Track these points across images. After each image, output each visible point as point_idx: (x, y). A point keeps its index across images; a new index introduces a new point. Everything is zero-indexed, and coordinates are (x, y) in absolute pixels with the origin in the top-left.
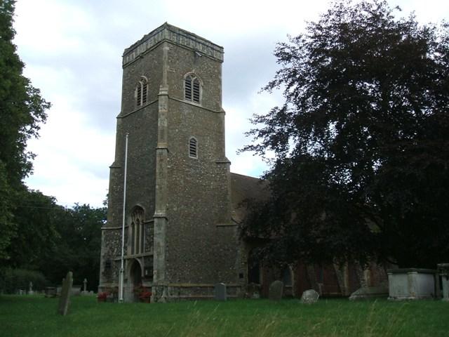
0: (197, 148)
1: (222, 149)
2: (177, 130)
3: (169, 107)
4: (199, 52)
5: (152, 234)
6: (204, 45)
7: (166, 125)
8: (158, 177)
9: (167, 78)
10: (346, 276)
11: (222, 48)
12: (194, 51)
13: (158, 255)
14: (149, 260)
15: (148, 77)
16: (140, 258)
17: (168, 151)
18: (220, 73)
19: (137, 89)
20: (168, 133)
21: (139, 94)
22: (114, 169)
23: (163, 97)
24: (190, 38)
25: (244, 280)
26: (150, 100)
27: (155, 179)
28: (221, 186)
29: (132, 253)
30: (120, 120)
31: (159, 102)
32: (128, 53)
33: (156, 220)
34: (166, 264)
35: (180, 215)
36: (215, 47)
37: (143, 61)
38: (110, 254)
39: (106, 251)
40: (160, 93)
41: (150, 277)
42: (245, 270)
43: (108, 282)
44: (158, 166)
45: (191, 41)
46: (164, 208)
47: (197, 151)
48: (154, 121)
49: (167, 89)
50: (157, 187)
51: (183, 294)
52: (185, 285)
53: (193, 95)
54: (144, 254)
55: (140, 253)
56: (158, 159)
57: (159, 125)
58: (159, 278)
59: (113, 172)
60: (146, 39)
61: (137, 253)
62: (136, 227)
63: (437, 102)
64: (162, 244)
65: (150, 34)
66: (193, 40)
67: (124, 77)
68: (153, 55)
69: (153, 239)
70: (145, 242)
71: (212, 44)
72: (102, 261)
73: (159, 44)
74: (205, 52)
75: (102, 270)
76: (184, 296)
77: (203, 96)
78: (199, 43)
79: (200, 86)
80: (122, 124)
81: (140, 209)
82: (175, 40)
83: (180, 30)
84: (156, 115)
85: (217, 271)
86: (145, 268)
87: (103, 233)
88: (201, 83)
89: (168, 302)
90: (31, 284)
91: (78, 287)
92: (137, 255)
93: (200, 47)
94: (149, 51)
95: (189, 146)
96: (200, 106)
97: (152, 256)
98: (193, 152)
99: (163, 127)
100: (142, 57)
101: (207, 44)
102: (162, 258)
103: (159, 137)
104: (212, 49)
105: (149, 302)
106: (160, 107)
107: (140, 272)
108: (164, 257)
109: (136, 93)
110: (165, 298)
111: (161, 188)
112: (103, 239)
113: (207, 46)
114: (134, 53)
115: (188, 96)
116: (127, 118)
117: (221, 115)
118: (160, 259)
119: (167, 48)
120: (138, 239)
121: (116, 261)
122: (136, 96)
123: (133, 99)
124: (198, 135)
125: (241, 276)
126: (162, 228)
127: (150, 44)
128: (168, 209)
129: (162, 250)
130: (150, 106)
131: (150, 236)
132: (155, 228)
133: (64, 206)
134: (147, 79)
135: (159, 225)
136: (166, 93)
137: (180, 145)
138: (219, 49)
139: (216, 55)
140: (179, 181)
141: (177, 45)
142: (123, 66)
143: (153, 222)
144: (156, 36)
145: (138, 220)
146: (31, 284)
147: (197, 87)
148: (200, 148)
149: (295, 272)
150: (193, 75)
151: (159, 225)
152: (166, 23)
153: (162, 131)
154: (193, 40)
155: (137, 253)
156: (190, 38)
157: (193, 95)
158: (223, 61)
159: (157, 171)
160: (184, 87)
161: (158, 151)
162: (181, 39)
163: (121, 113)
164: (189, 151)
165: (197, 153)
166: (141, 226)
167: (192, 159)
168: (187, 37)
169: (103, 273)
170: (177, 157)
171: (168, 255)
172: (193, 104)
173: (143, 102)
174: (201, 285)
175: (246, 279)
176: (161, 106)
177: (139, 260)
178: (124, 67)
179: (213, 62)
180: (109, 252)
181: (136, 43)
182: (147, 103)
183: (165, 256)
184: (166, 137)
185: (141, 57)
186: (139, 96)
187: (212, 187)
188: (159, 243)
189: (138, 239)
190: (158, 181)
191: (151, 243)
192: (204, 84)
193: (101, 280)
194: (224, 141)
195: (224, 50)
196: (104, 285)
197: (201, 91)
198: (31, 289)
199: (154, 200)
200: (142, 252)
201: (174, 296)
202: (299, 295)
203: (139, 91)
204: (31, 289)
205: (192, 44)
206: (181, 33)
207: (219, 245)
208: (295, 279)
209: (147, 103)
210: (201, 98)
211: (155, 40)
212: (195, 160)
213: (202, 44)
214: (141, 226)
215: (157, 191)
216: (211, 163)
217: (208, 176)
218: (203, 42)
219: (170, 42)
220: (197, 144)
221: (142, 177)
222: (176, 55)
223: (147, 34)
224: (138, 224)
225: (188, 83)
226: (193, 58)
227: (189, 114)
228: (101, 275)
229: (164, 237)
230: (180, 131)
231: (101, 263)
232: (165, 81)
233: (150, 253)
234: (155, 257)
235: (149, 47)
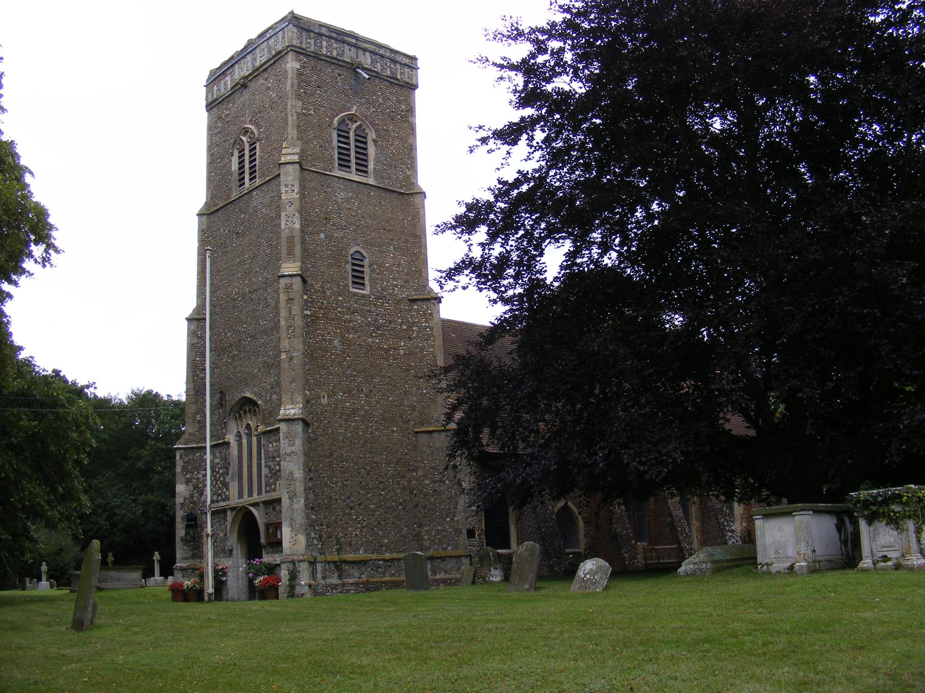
0: (366, 270)
1: (420, 271)
2: (322, 236)
3: (303, 187)
4: (363, 69)
5: (275, 457)
6: (377, 54)
7: (297, 226)
8: (283, 335)
9: (304, 126)
10: (696, 524)
11: (414, 59)
12: (353, 68)
13: (290, 498)
14: (274, 509)
15: (258, 126)
16: (255, 505)
17: (304, 281)
18: (411, 110)
19: (236, 154)
20: (303, 242)
21: (241, 163)
22: (195, 323)
23: (289, 168)
24: (344, 42)
25: (476, 541)
26: (263, 175)
27: (279, 339)
28: (422, 349)
29: (241, 496)
30: (205, 218)
31: (282, 178)
32: (216, 77)
33: (283, 427)
34: (308, 516)
35: (334, 414)
36: (399, 58)
37: (246, 94)
38: (195, 499)
39: (187, 495)
40: (283, 160)
41: (277, 545)
42: (480, 521)
43: (194, 556)
44: (283, 313)
45: (347, 48)
46: (299, 399)
47: (367, 278)
48: (273, 219)
49: (298, 150)
50: (283, 356)
51: (349, 576)
52: (350, 557)
53: (353, 160)
54: (265, 497)
55: (255, 495)
56: (283, 298)
57: (283, 226)
58: (293, 540)
59: (192, 327)
60: (250, 48)
61: (250, 495)
62: (245, 441)
63: (559, 188)
64: (299, 474)
65: (261, 35)
66: (349, 44)
67: (210, 128)
68: (266, 79)
69: (279, 465)
70: (265, 471)
71: (392, 51)
72: (180, 514)
73: (279, 56)
74: (378, 68)
75: (180, 532)
76: (351, 581)
77: (377, 161)
78: (365, 50)
79: (369, 139)
80: (209, 227)
81: (252, 403)
82: (313, 48)
83: (321, 25)
84: (276, 205)
85: (420, 526)
86: (268, 526)
87: (178, 457)
88: (372, 135)
89: (315, 593)
90: (44, 568)
91: (137, 569)
92: (256, 497)
93: (366, 60)
94: (258, 72)
95: (349, 267)
96: (371, 181)
97: (279, 501)
98: (359, 280)
99: (292, 229)
100: (244, 86)
101: (382, 52)
102: (300, 504)
103: (284, 251)
104: (395, 62)
105: (277, 597)
106: (283, 189)
107: (255, 535)
108: (303, 500)
109: (235, 161)
110: (310, 586)
111: (291, 359)
112: (178, 469)
113: (382, 56)
114: (228, 78)
115: (344, 164)
116: (219, 214)
117: (417, 199)
118: (296, 506)
119: (297, 65)
120: (250, 467)
121: (267, 503)
122: (235, 166)
123: (230, 173)
124: (368, 244)
125: (471, 534)
126: (298, 442)
127: (261, 57)
128: (308, 402)
129: (299, 487)
130: (264, 188)
131: (274, 458)
132: (284, 443)
133: (113, 395)
134: (256, 132)
135: (290, 436)
136: (296, 158)
137: (330, 266)
138: (407, 61)
139: (402, 74)
140: (331, 341)
141: (316, 56)
142: (207, 106)
143: (278, 429)
144: (271, 42)
145: (248, 425)
146: (44, 568)
147: (361, 141)
148: (373, 271)
149: (586, 522)
150: (352, 118)
151: (290, 436)
152: (292, 13)
153: (290, 239)
154: (349, 44)
155: (250, 495)
156: (266, 69)
157: (353, 160)
158: (416, 87)
159: (283, 323)
160: (335, 143)
161: (283, 282)
162: (324, 43)
163: (206, 203)
164: (350, 279)
165: (367, 282)
166: (254, 439)
167: (355, 294)
168: (336, 40)
169: (182, 540)
170: (324, 292)
171: (311, 496)
172: (357, 178)
173: (251, 180)
174: (388, 556)
175: (480, 536)
176: (286, 186)
177: (251, 508)
178: (210, 106)
179: (395, 89)
180: (192, 496)
181: (232, 58)
182: (258, 182)
183: (307, 499)
184: (298, 249)
185: (243, 85)
186: (241, 167)
187: (402, 352)
188: (291, 473)
189: (250, 467)
190: (285, 344)
191: (275, 474)
192: (379, 135)
193: (179, 554)
194: (426, 254)
195: (420, 64)
196: (184, 565)
197: (372, 150)
198: (44, 577)
199: (278, 384)
200: (260, 493)
201: (329, 581)
202: (570, 573)
203: (241, 156)
204: (44, 577)
205: (349, 55)
206: (324, 31)
207: (420, 472)
208: (585, 535)
209: (258, 182)
210: (371, 166)
211: (270, 48)
212: (363, 296)
213: (371, 52)
214: (254, 439)
215: (285, 366)
216: (399, 302)
217: (393, 329)
218: (372, 48)
219: (300, 52)
220: (366, 262)
221: (253, 337)
222: (315, 77)
223: (254, 36)
224: (249, 435)
225: (343, 135)
226: (352, 81)
227: (348, 200)
228: (179, 544)
229: (301, 461)
230: (329, 237)
231: (178, 519)
232: (292, 132)
233: (274, 495)
234: (285, 501)
235: (258, 64)
